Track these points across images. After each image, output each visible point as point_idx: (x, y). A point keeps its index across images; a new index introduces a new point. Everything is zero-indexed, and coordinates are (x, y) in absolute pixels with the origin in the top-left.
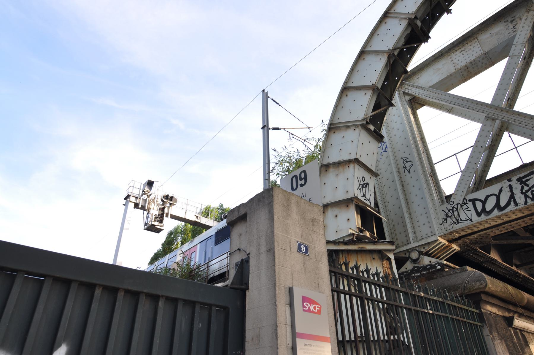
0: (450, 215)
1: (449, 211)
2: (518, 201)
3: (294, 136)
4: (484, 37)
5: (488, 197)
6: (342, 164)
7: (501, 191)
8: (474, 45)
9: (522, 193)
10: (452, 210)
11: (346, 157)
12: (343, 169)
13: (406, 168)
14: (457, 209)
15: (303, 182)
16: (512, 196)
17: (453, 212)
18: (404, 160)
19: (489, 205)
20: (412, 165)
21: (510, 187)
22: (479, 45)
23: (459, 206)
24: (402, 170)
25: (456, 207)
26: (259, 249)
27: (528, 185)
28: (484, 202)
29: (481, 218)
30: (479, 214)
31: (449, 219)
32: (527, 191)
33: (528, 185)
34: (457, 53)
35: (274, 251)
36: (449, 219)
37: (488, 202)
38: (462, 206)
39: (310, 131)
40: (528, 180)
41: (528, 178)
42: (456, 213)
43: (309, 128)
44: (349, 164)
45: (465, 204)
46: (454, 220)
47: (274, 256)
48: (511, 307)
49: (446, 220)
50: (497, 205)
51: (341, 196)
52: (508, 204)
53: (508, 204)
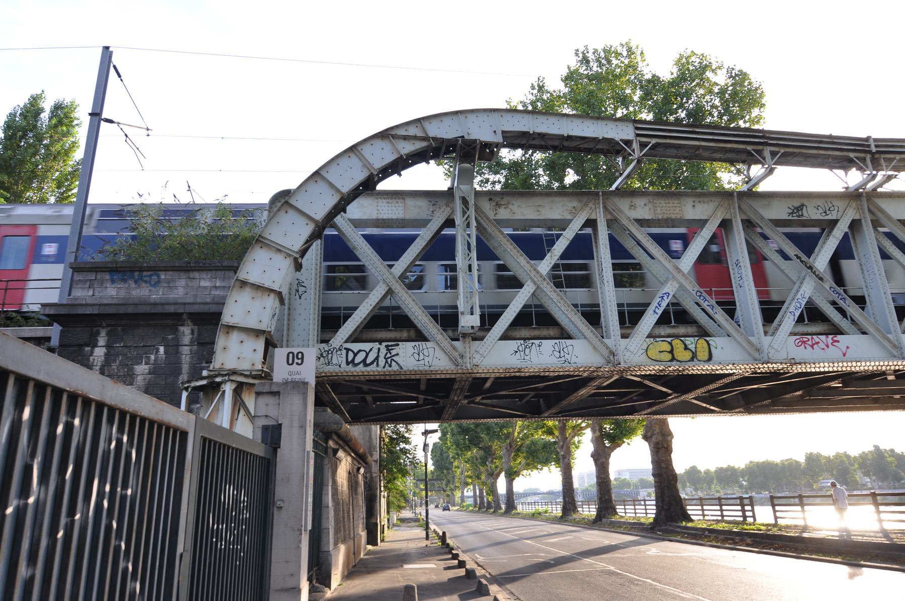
0: (325, 355)
1: (325, 351)
2: (380, 363)
3: (128, 140)
4: (410, 202)
5: (360, 351)
6: (262, 289)
7: (371, 350)
8: (399, 204)
9: (385, 358)
10: (328, 352)
11: (268, 284)
12: (262, 295)
13: (298, 292)
14: (332, 352)
15: (300, 361)
16: (377, 358)
17: (328, 353)
18: (299, 282)
19: (359, 359)
20: (306, 292)
21: (379, 349)
22: (403, 208)
23: (335, 350)
24: (293, 292)
25: (332, 350)
26: (292, 423)
27: (390, 353)
28: (355, 355)
29: (348, 367)
30: (348, 363)
31: (322, 359)
32: (389, 358)
33: (390, 353)
34: (385, 201)
35: (306, 429)
36: (322, 359)
37: (358, 355)
38: (337, 351)
39: (148, 135)
40: (392, 349)
41: (393, 348)
42: (330, 356)
43: (148, 129)
44: (270, 292)
45: (340, 350)
46: (327, 361)
47: (305, 432)
48: (341, 443)
49: (319, 358)
50: (364, 361)
51: (252, 323)
52: (372, 363)
53: (372, 363)
